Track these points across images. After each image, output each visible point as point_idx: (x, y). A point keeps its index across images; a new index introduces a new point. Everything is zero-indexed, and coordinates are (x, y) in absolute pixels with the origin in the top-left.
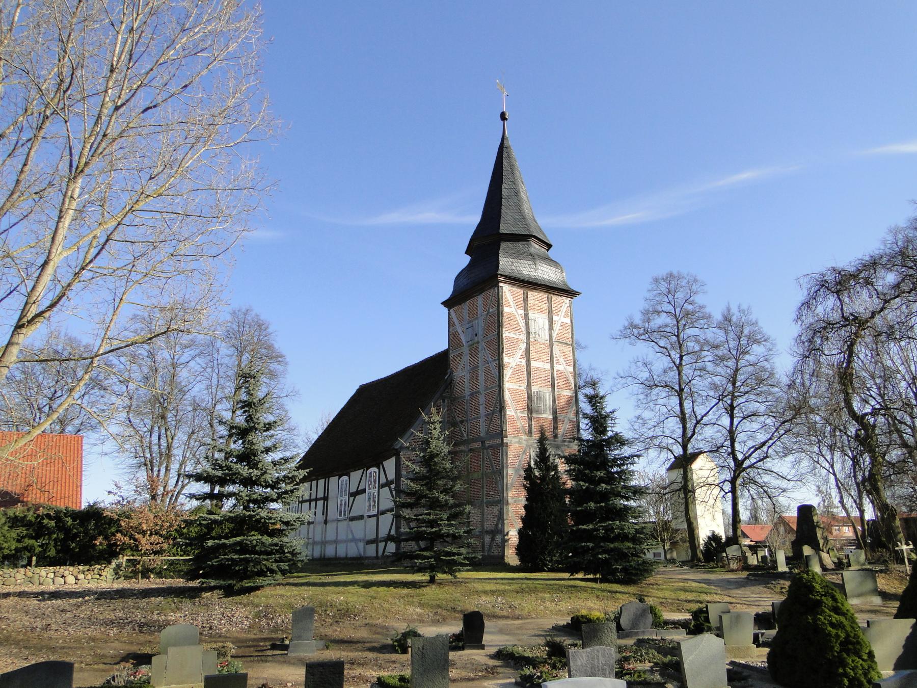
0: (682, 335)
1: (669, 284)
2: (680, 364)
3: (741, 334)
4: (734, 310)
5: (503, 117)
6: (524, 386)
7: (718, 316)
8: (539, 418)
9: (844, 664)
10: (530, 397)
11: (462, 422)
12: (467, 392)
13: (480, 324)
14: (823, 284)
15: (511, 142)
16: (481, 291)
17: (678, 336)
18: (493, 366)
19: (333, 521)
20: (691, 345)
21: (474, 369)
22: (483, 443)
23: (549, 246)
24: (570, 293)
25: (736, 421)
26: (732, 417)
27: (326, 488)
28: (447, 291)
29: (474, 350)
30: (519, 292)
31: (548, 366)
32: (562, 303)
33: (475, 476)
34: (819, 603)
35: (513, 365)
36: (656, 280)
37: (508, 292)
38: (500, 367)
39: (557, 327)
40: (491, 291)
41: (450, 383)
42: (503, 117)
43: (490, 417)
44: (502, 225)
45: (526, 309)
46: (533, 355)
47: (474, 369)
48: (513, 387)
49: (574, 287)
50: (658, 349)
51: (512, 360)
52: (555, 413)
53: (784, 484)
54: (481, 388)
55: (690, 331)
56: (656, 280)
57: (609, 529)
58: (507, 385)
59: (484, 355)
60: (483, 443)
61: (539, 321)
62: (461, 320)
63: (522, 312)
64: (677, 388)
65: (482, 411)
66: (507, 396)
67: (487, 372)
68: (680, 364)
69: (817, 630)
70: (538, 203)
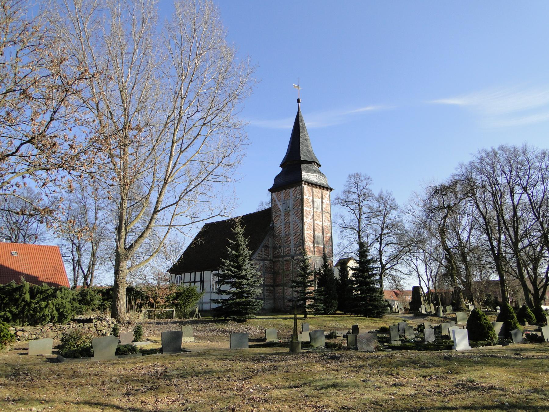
0: (361, 204)
1: (356, 179)
2: (360, 218)
3: (386, 204)
4: (384, 193)
5: (298, 101)
6: (312, 232)
7: (376, 195)
8: (318, 247)
9: (489, 333)
10: (314, 238)
11: (280, 247)
12: (283, 234)
13: (291, 202)
14: (436, 191)
15: (302, 114)
16: (292, 187)
17: (359, 205)
18: (299, 222)
19: (207, 292)
20: (365, 209)
21: (287, 224)
22: (293, 258)
23: (320, 166)
24: (329, 189)
25: (383, 245)
26: (381, 244)
27: (202, 277)
28: (271, 185)
29: (287, 213)
30: (310, 188)
31: (321, 223)
32: (326, 193)
33: (288, 272)
34: (481, 318)
35: (308, 222)
36: (350, 177)
37: (306, 189)
38: (303, 223)
39: (324, 205)
40: (298, 188)
41: (273, 228)
42: (298, 101)
43: (296, 246)
44: (301, 156)
45: (313, 197)
46: (315, 218)
47: (287, 224)
48: (308, 232)
49: (331, 187)
50: (350, 210)
51: (308, 220)
52: (324, 245)
53: (403, 276)
54: (292, 231)
55: (365, 202)
56: (350, 177)
57: (371, 297)
58: (306, 232)
59: (293, 217)
60: (293, 258)
61: (318, 201)
62: (279, 199)
63: (311, 198)
64: (358, 230)
65: (292, 243)
66: (306, 236)
67: (295, 225)
68: (360, 218)
69: (481, 324)
70: (314, 145)
